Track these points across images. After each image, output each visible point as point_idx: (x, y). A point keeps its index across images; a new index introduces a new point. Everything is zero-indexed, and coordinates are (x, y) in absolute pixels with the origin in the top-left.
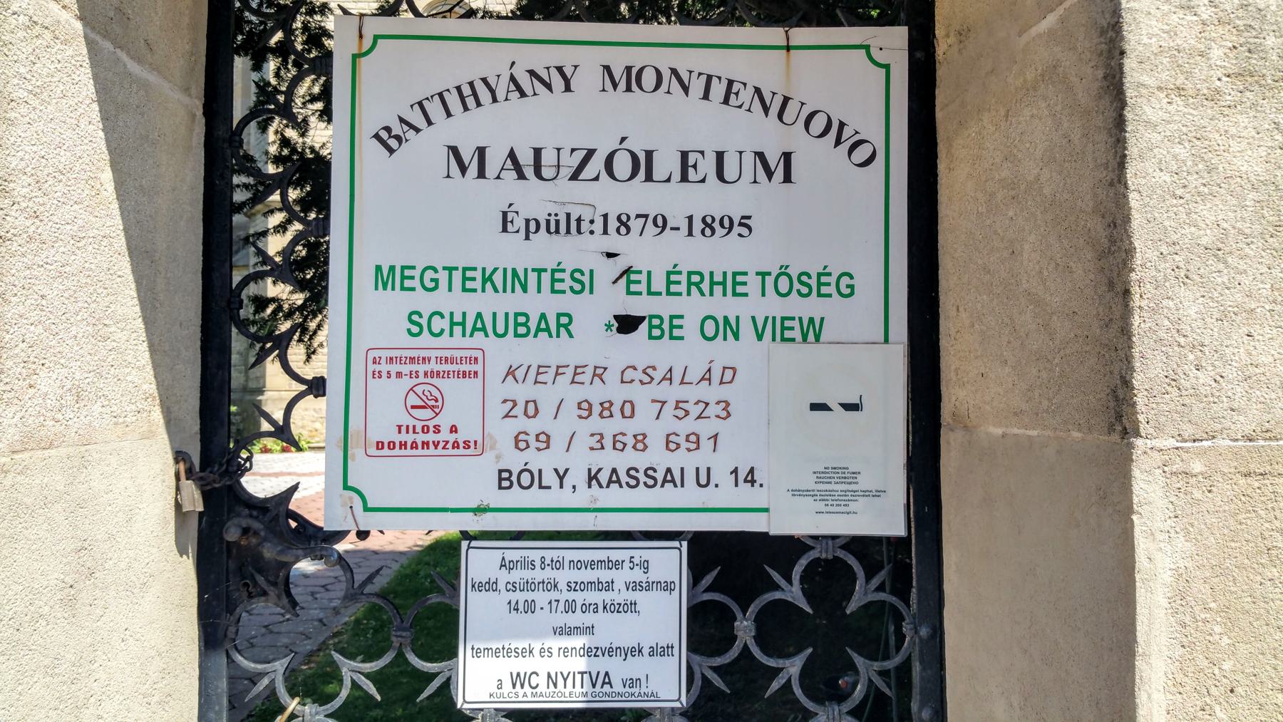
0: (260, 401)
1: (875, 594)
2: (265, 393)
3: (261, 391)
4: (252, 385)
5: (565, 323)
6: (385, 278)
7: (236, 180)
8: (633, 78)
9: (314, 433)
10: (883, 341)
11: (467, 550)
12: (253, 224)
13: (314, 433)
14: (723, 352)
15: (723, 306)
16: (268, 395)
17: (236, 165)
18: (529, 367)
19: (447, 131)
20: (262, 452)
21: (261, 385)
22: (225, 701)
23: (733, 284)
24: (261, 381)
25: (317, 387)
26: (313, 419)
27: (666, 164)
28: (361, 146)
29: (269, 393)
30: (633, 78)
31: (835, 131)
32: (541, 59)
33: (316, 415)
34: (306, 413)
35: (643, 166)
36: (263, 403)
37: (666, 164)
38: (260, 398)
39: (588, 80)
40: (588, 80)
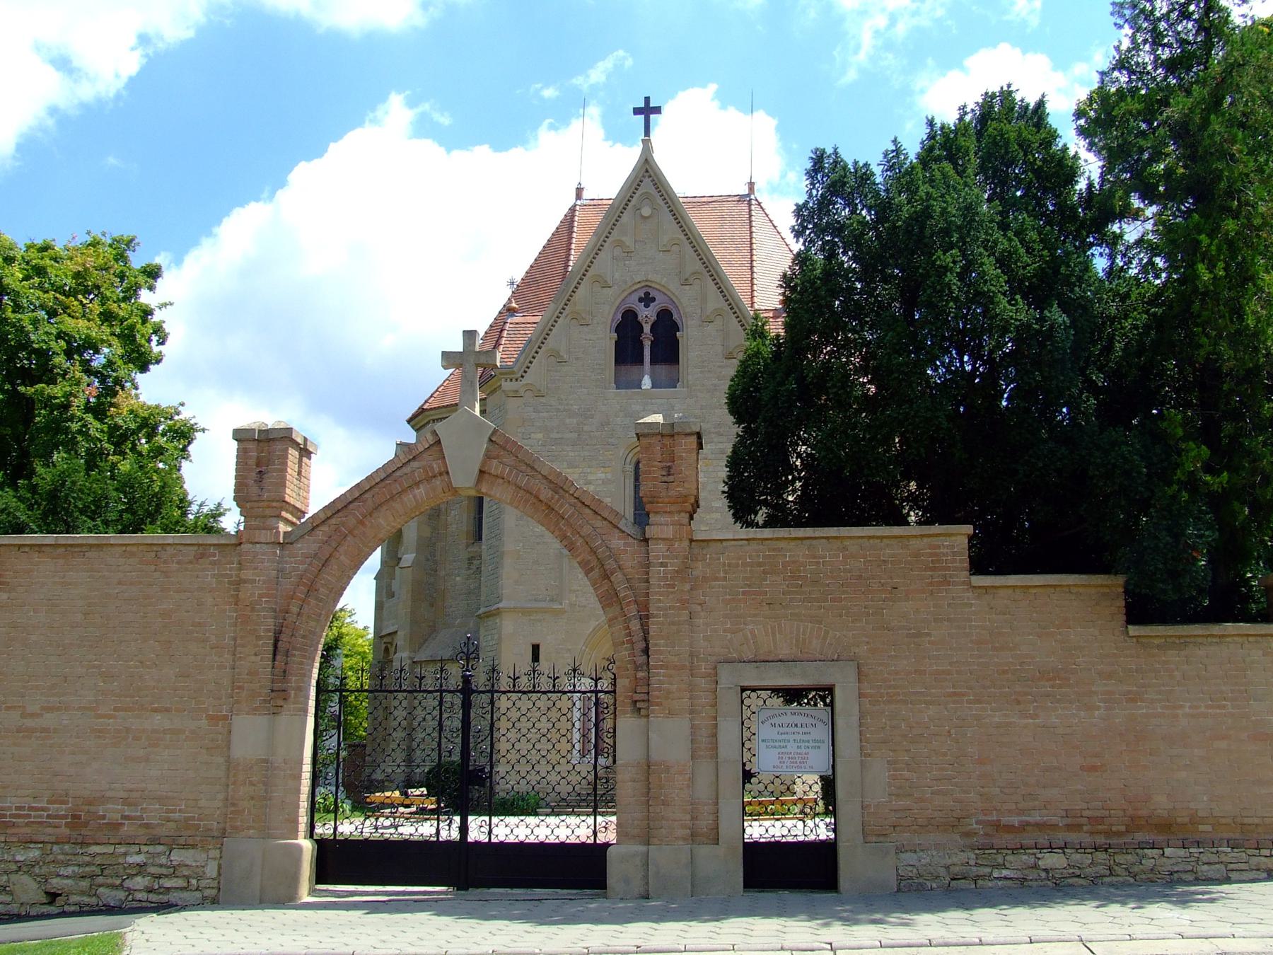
0: (445, 368)
5: (786, 746)
6: (763, 741)
8: (795, 714)
11: (935, 946)
14: (807, 750)
15: (807, 744)
17: (992, 517)
19: (770, 721)
23: (809, 741)
25: (754, 755)
27: (799, 725)
28: (373, 908)
30: (795, 714)
31: (822, 721)
32: (782, 711)
35: (796, 725)
37: (799, 725)
39: (789, 714)
40: (789, 714)
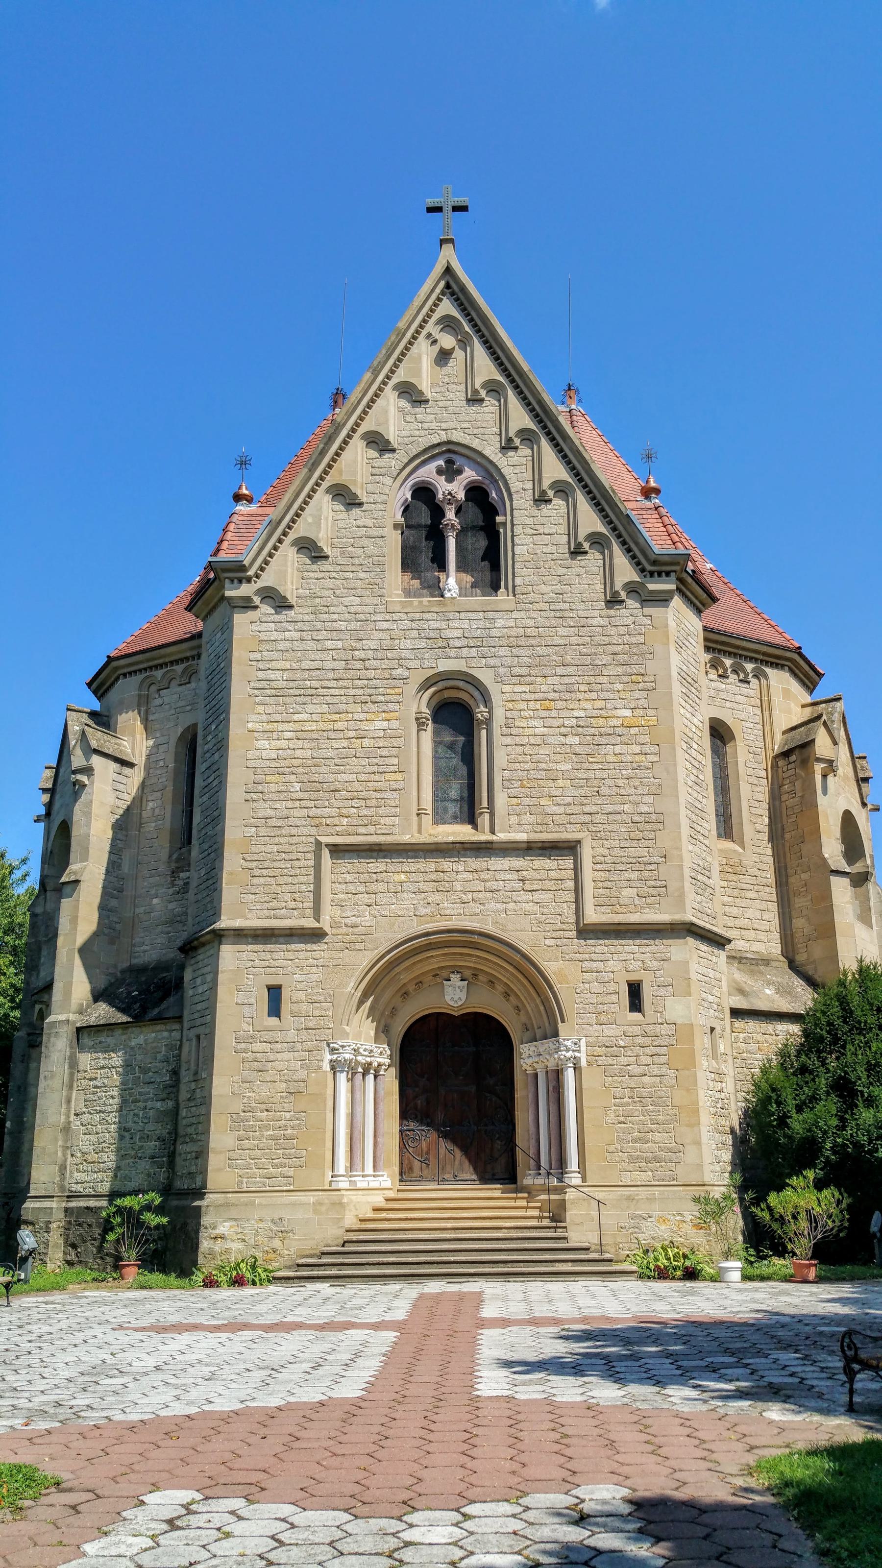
0: (200, 1207)
1: (444, 262)
2: (206, 1197)
3: (199, 1193)
4: (181, 1184)
7: (837, 1464)
9: (272, 1256)
10: (569, 863)
12: (193, 961)
13: (272, 1256)
16: (209, 1199)
18: (566, 1238)
20: (205, 1286)
21: (199, 1184)
22: (873, 912)
24: (199, 1179)
26: (271, 1234)
29: (211, 1195)
33: (275, 1228)
34: (261, 1225)
36: (203, 1210)
38: (196, 1203)
